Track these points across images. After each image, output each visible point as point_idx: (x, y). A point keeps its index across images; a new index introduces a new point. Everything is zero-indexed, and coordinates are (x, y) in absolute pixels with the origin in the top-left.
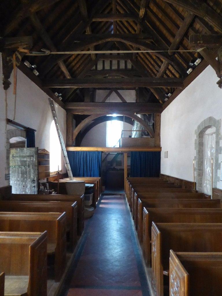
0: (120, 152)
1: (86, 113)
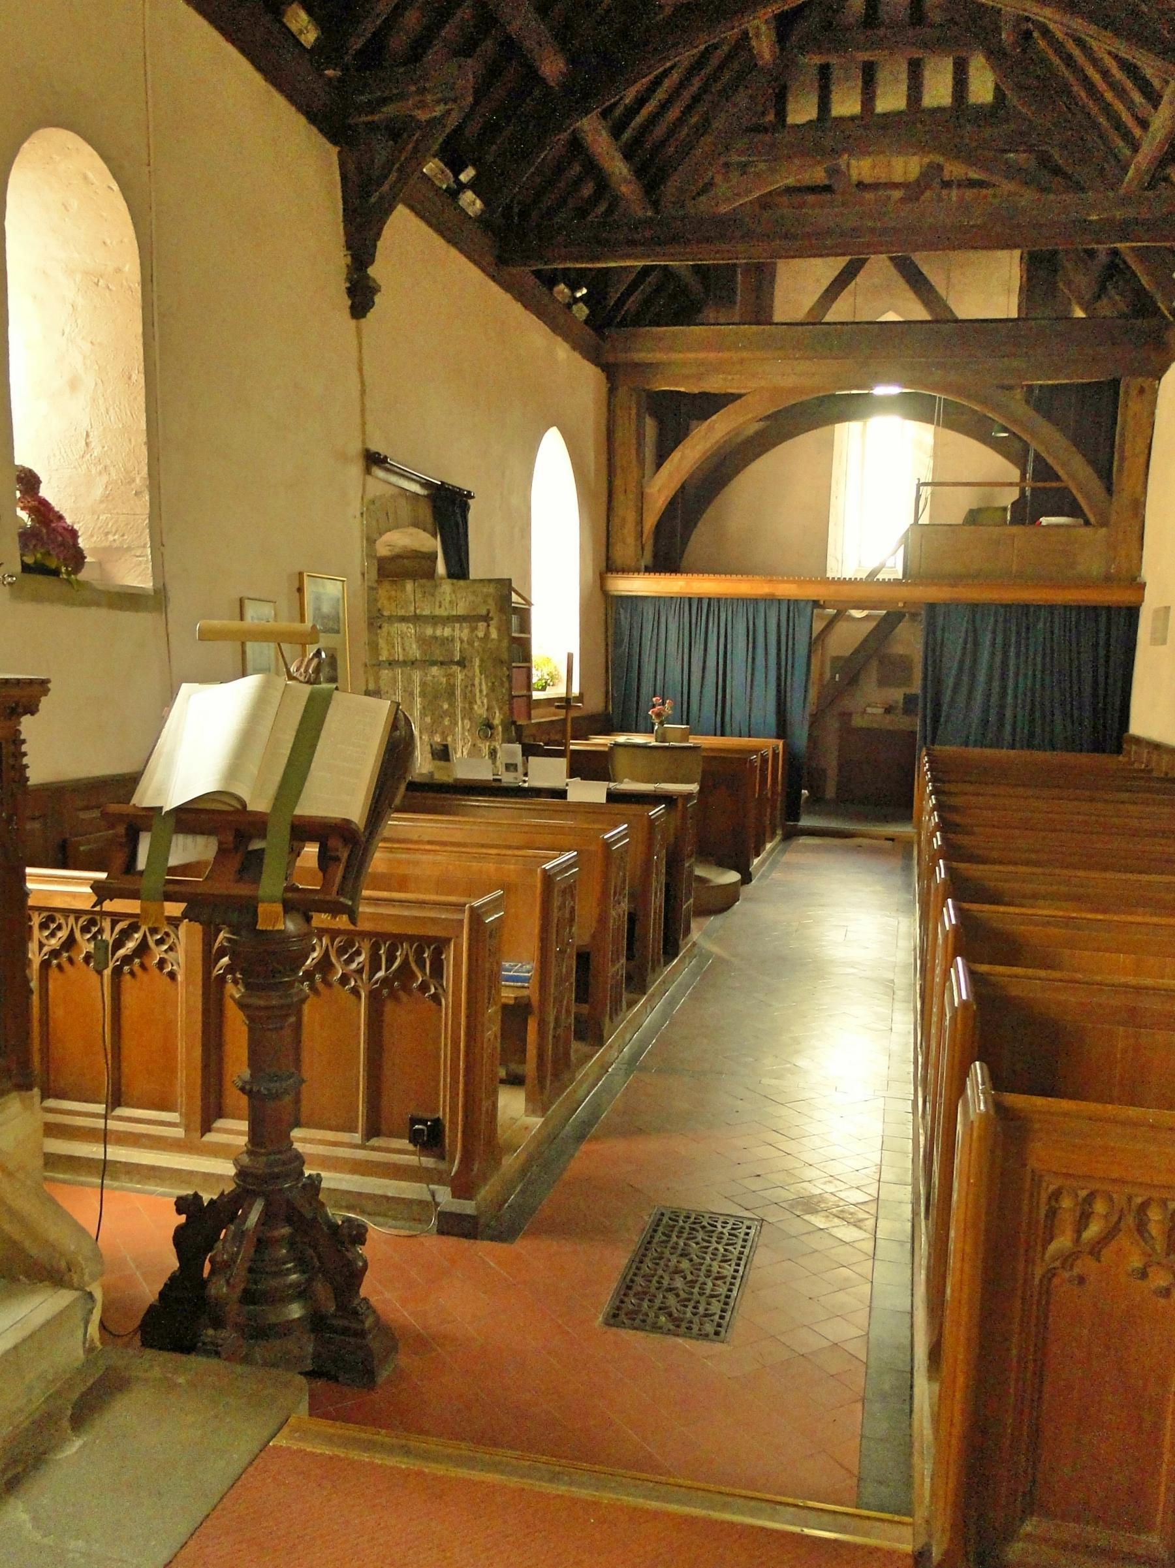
0: (901, 605)
1: (714, 384)
